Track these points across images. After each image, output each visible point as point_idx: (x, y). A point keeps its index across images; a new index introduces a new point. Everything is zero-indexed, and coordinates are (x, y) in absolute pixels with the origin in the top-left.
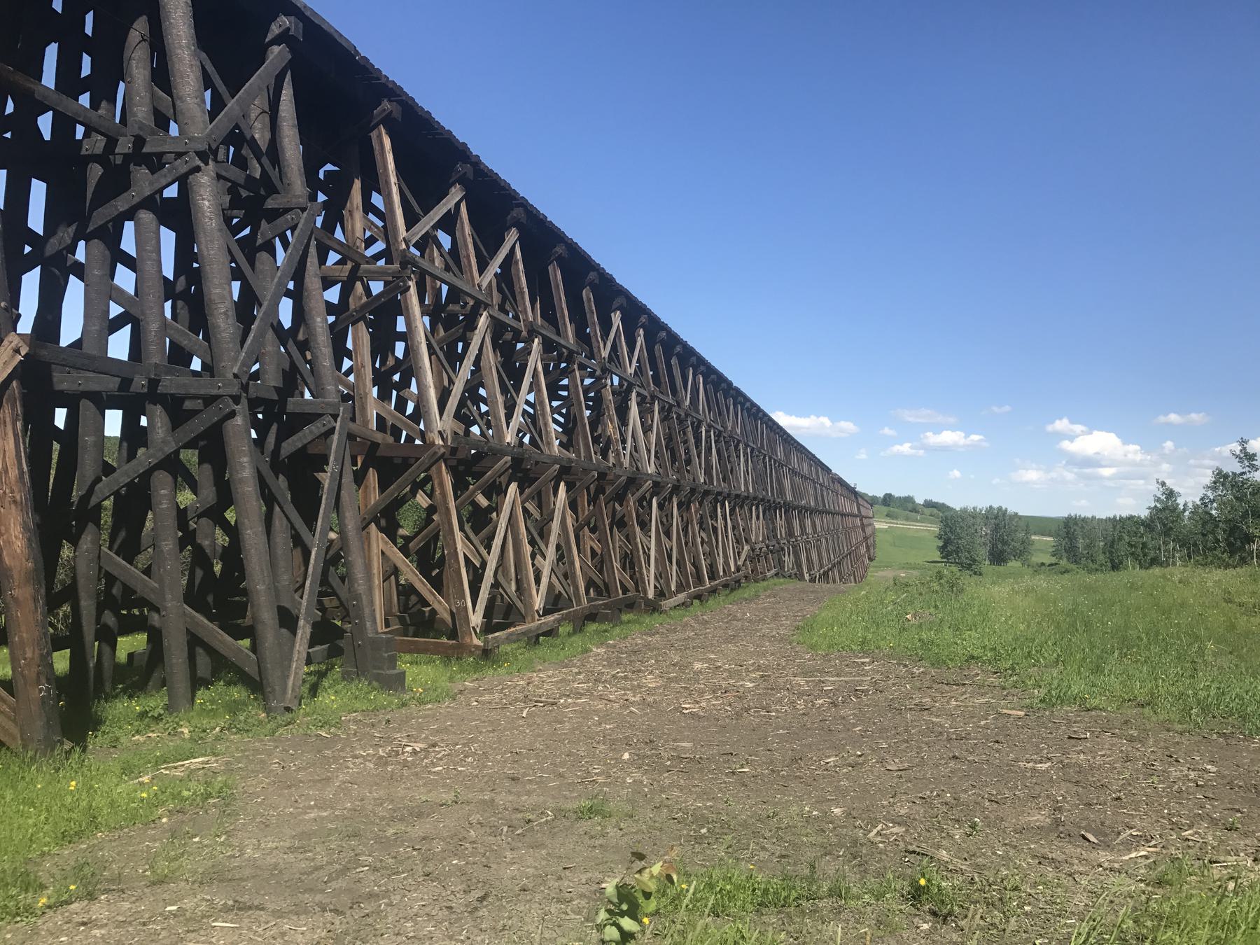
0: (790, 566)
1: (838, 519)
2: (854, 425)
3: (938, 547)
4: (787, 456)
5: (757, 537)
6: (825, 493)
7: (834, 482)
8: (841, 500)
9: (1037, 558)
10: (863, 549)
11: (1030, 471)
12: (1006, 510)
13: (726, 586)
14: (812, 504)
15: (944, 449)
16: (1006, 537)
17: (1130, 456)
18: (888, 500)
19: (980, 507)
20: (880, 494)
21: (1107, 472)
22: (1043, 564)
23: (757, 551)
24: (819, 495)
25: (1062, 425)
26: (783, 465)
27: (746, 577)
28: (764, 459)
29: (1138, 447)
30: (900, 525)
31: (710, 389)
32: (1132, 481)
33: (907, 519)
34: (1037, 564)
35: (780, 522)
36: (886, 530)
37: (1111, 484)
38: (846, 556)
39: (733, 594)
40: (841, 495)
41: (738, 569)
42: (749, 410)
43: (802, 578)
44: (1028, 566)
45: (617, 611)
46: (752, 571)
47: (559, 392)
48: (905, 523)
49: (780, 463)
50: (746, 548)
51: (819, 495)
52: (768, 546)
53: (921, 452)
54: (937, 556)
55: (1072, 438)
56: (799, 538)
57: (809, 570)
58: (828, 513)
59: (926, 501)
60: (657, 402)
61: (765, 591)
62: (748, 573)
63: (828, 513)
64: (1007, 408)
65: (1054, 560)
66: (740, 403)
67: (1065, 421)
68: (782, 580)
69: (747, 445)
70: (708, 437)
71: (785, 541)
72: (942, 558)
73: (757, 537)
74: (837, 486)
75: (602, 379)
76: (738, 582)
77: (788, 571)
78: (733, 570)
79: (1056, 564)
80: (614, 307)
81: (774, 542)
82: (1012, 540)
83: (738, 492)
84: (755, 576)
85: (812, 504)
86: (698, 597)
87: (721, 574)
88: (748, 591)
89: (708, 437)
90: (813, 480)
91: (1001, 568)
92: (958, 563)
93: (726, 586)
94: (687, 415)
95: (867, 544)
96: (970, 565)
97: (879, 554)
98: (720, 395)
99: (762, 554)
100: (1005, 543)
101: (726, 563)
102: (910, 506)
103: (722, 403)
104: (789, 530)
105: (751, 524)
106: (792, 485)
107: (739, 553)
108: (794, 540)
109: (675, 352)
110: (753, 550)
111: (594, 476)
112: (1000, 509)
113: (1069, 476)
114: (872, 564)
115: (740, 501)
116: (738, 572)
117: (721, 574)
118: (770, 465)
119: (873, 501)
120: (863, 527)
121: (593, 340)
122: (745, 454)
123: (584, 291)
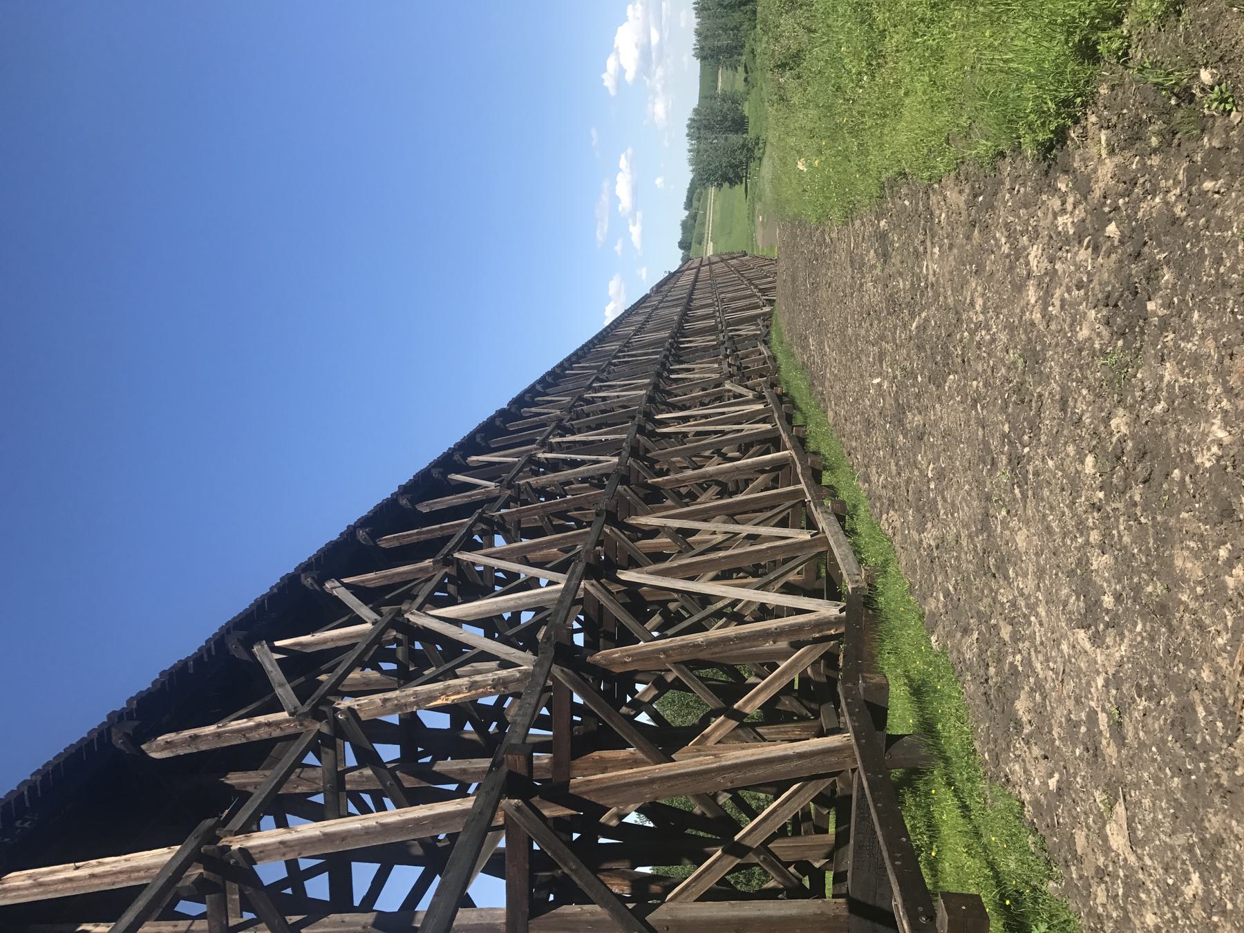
0: (754, 327)
1: (699, 285)
2: (612, 279)
3: (730, 188)
4: (619, 338)
5: (713, 371)
6: (669, 299)
7: (661, 292)
8: (679, 283)
9: (740, 86)
10: (734, 262)
11: (655, 111)
12: (690, 119)
13: (789, 419)
14: (679, 309)
15: (635, 191)
16: (719, 118)
17: (639, 14)
18: (685, 245)
19: (688, 146)
20: (680, 253)
21: (655, 38)
22: (746, 80)
23: (734, 370)
24: (668, 304)
25: (609, 80)
26: (628, 343)
27: (773, 386)
28: (615, 365)
29: (630, 7)
30: (709, 230)
31: (495, 443)
32: (663, 12)
33: (704, 224)
34: (746, 86)
35: (699, 342)
36: (715, 243)
37: (666, 36)
38: (742, 274)
39: (802, 406)
40: (675, 284)
41: (760, 398)
42: (550, 385)
43: (770, 314)
44: (748, 94)
45: (896, 750)
46: (762, 376)
47: (420, 761)
48: (707, 225)
49: (625, 346)
50: (728, 386)
51: (668, 304)
52: (727, 356)
53: (639, 214)
54: (739, 189)
55: (622, 71)
56: (719, 320)
57: (758, 307)
58: (691, 293)
59: (685, 209)
60: (457, 555)
61: (793, 355)
62: (766, 382)
63: (691, 293)
64: (594, 133)
65: (741, 69)
66: (532, 398)
67: (604, 76)
68: (774, 335)
69: (590, 388)
70: (559, 447)
71: (721, 335)
72: (742, 183)
73: (713, 371)
74: (666, 288)
75: (336, 719)
76: (780, 398)
77: (760, 330)
78: (761, 407)
79: (746, 67)
80: (245, 657)
81: (722, 348)
82: (721, 111)
83: (644, 399)
84: (770, 371)
85: (679, 309)
86: (816, 476)
87: (769, 426)
88: (796, 383)
89: (559, 447)
90: (653, 310)
91: (751, 121)
92: (747, 166)
93: (789, 419)
94: (510, 486)
95: (728, 259)
96: (748, 150)
97: (738, 249)
98: (512, 426)
99: (738, 363)
100: (725, 118)
101: (750, 418)
102: (690, 222)
103: (523, 424)
104: (708, 331)
105: (698, 379)
106: (653, 332)
107: (735, 397)
108: (720, 325)
109: (409, 506)
110: (731, 376)
111: (518, 808)
112: (689, 126)
113: (660, 72)
114: (749, 252)
115: (659, 396)
116: (764, 397)
117: (769, 426)
118: (624, 357)
119: (686, 260)
120: (710, 264)
121: (255, 736)
122: (600, 389)
123: (154, 755)
